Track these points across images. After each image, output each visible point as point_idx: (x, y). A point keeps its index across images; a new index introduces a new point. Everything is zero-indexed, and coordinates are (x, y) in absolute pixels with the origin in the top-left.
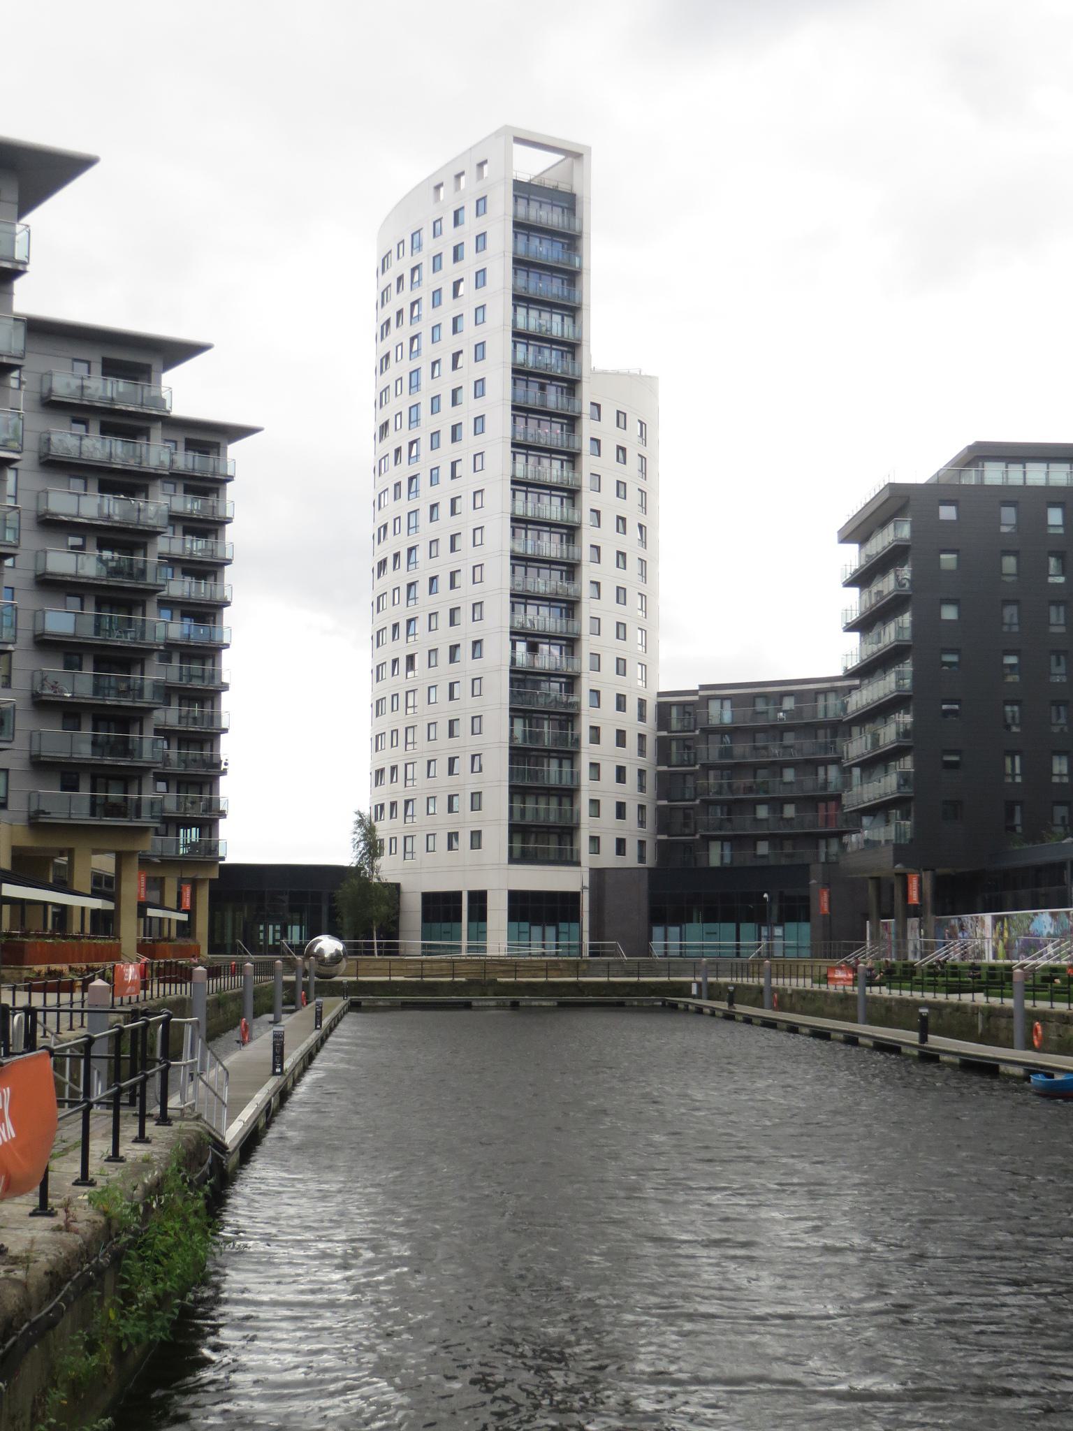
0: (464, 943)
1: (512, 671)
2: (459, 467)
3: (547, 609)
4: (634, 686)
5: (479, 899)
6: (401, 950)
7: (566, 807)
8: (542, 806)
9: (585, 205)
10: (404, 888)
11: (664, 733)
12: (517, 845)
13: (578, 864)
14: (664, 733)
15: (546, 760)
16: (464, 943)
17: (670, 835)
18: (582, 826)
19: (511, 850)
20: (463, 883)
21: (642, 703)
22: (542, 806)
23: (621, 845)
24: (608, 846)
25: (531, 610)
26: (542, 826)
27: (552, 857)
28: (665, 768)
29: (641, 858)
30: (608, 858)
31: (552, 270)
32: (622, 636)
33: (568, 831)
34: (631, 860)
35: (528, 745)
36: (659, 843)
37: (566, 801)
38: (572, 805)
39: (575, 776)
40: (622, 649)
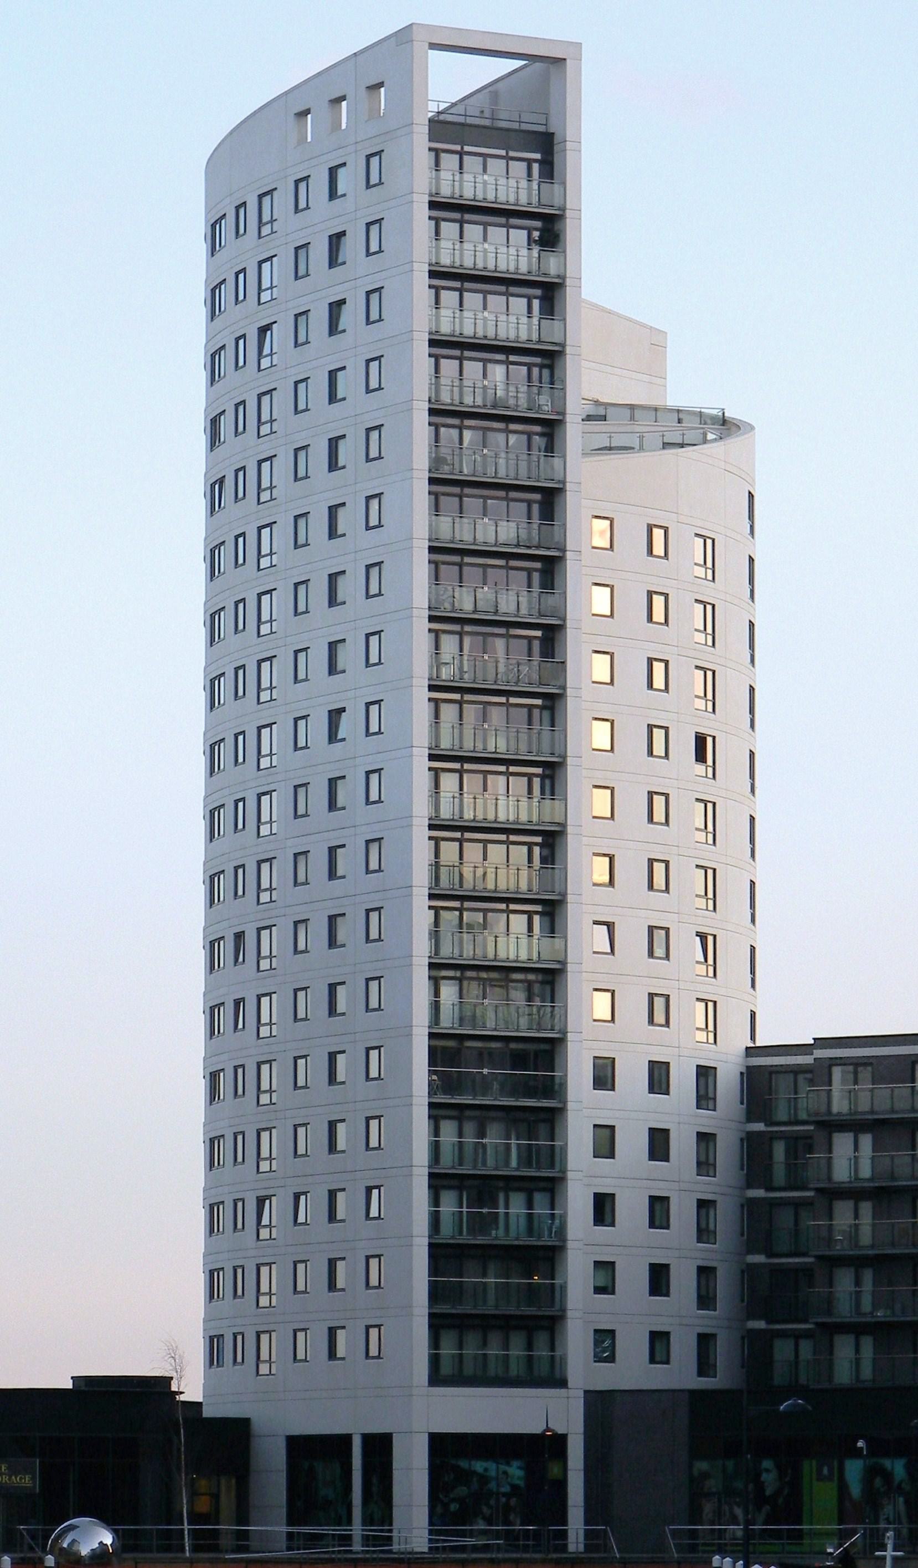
0: (357, 1529)
1: (431, 1036)
2: (341, 652)
3: (502, 780)
4: (685, 1046)
5: (379, 1447)
6: (253, 1544)
7: (541, 1210)
8: (494, 1351)
9: (570, 156)
10: (256, 1427)
11: (759, 1127)
12: (448, 1350)
13: (562, 1383)
14: (759, 1127)
15: (501, 1197)
16: (357, 1529)
17: (770, 1255)
18: (570, 1314)
19: (435, 1361)
20: (349, 1419)
21: (705, 1074)
22: (494, 1351)
23: (659, 1343)
24: (632, 1346)
25: (473, 851)
26: (494, 1289)
27: (513, 1371)
28: (760, 1193)
29: (705, 1366)
30: (632, 1371)
31: (505, 1324)
32: (659, 1017)
33: (545, 1322)
34: (680, 1373)
35: (466, 1239)
36: (749, 1272)
37: (541, 1339)
38: (553, 1348)
39: (553, 1157)
40: (660, 976)
